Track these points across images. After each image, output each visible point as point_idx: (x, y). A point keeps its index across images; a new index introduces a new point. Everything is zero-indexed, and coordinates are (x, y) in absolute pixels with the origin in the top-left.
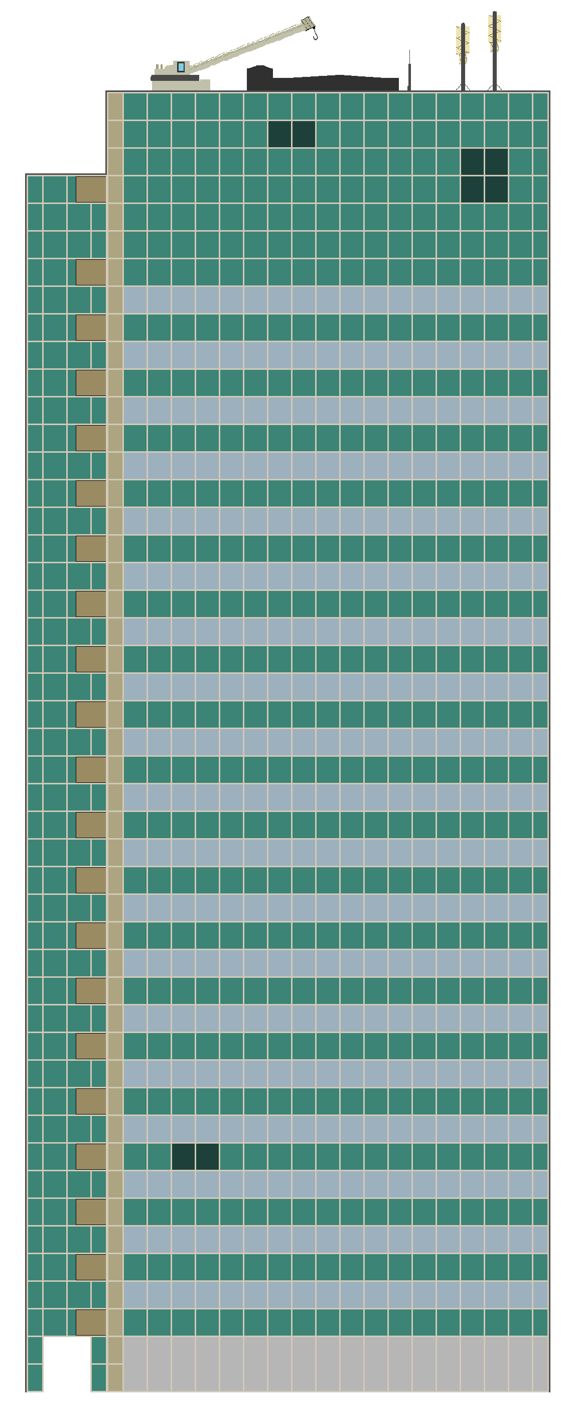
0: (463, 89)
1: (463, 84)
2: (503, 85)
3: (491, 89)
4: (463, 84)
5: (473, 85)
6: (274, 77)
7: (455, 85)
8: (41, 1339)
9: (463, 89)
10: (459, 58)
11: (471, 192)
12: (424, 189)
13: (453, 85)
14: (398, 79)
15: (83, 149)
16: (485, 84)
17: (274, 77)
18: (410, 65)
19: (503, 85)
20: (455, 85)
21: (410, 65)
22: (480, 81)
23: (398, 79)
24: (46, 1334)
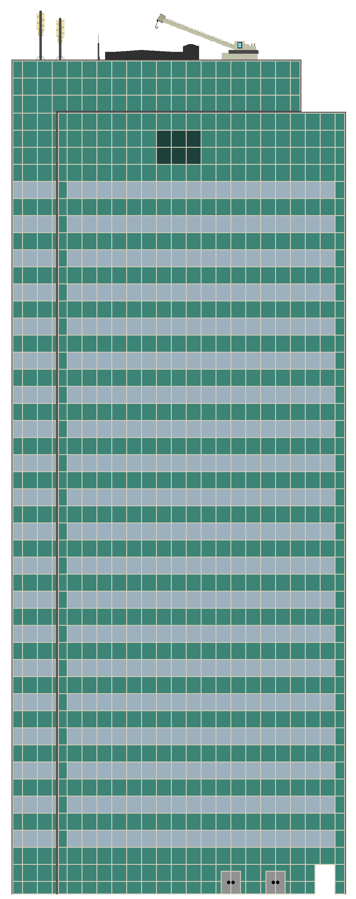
0: (60, 59)
1: (60, 56)
2: (65, 56)
3: (58, 59)
4: (60, 56)
5: (46, 56)
6: (182, 51)
7: (36, 56)
8: (333, 863)
9: (60, 59)
10: (58, 38)
11: (163, 137)
12: (223, 139)
13: (35, 56)
14: (106, 53)
15: (314, 99)
16: (54, 56)
17: (182, 51)
18: (98, 44)
19: (65, 56)
20: (36, 56)
21: (98, 44)
22: (50, 54)
23: (106, 53)
24: (336, 866)
